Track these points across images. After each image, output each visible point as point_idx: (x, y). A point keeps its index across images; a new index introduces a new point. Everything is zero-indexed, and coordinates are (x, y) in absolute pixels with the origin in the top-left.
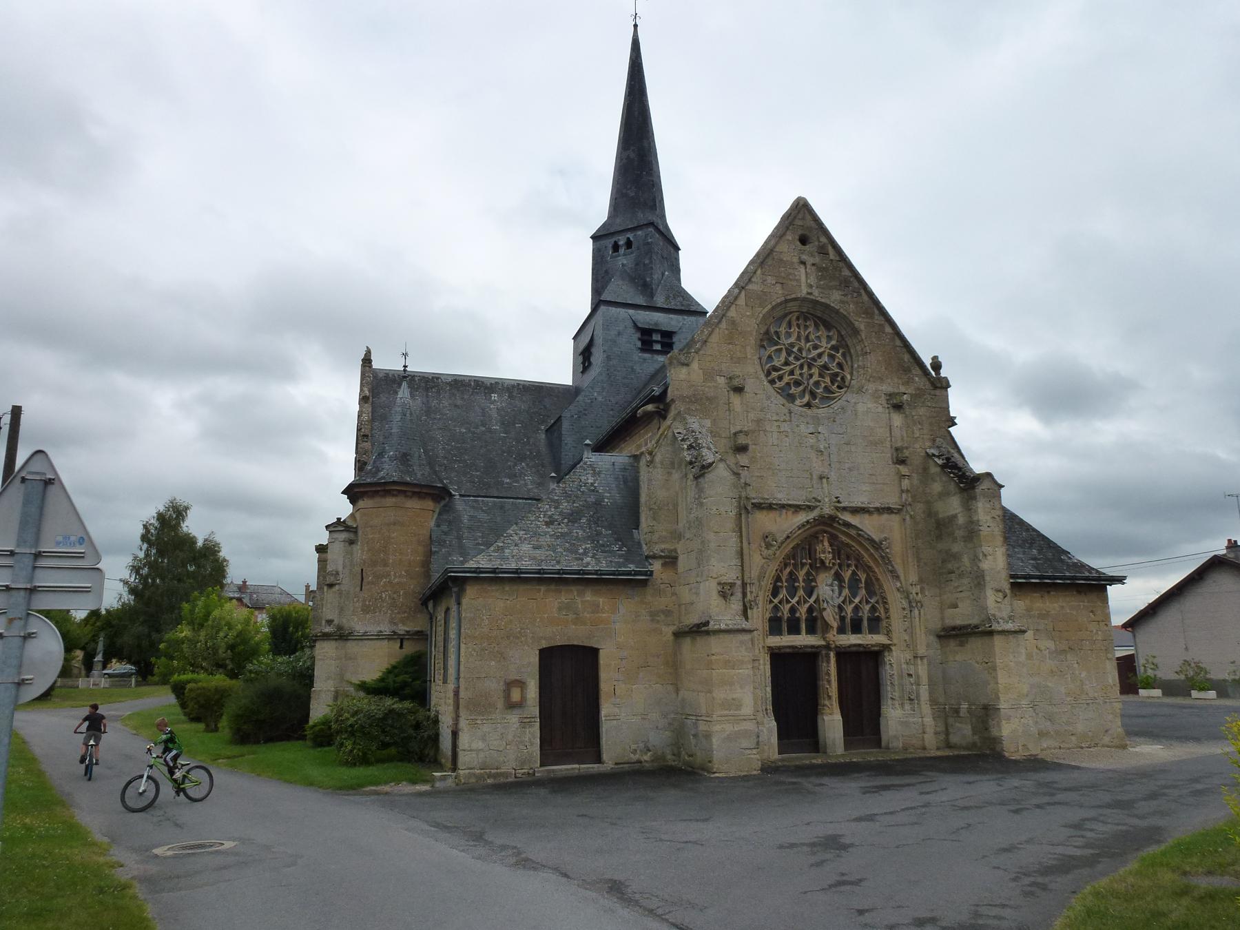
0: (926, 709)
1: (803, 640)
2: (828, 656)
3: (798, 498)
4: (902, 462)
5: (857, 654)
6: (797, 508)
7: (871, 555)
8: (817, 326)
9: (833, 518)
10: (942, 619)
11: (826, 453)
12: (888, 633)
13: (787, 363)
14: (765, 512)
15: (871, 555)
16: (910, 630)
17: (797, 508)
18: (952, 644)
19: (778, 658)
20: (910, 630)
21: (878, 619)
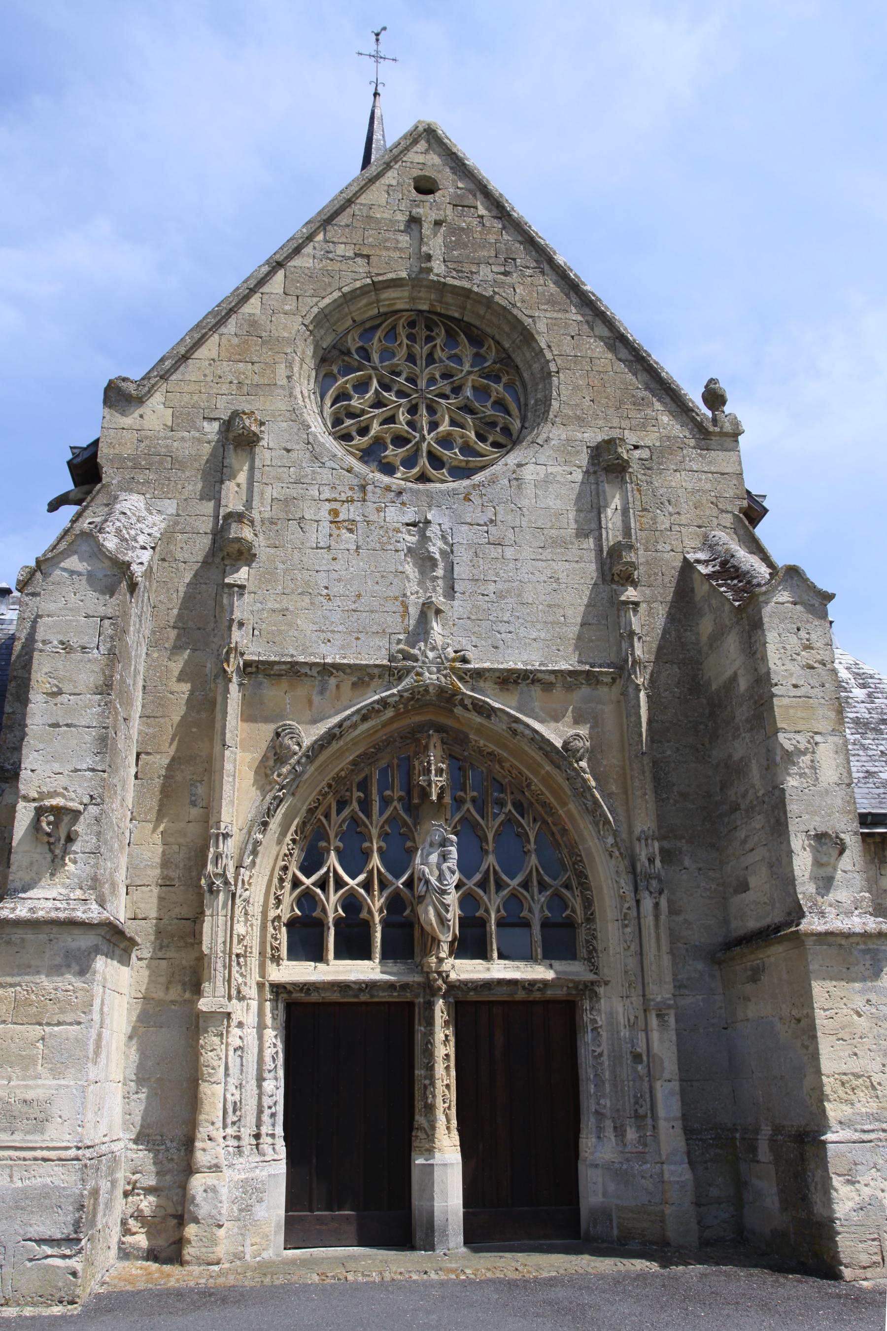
6: (362, 676)
8: (451, 336)
10: (726, 922)
12: (591, 959)
13: (379, 403)
14: (285, 684)
21: (570, 925)
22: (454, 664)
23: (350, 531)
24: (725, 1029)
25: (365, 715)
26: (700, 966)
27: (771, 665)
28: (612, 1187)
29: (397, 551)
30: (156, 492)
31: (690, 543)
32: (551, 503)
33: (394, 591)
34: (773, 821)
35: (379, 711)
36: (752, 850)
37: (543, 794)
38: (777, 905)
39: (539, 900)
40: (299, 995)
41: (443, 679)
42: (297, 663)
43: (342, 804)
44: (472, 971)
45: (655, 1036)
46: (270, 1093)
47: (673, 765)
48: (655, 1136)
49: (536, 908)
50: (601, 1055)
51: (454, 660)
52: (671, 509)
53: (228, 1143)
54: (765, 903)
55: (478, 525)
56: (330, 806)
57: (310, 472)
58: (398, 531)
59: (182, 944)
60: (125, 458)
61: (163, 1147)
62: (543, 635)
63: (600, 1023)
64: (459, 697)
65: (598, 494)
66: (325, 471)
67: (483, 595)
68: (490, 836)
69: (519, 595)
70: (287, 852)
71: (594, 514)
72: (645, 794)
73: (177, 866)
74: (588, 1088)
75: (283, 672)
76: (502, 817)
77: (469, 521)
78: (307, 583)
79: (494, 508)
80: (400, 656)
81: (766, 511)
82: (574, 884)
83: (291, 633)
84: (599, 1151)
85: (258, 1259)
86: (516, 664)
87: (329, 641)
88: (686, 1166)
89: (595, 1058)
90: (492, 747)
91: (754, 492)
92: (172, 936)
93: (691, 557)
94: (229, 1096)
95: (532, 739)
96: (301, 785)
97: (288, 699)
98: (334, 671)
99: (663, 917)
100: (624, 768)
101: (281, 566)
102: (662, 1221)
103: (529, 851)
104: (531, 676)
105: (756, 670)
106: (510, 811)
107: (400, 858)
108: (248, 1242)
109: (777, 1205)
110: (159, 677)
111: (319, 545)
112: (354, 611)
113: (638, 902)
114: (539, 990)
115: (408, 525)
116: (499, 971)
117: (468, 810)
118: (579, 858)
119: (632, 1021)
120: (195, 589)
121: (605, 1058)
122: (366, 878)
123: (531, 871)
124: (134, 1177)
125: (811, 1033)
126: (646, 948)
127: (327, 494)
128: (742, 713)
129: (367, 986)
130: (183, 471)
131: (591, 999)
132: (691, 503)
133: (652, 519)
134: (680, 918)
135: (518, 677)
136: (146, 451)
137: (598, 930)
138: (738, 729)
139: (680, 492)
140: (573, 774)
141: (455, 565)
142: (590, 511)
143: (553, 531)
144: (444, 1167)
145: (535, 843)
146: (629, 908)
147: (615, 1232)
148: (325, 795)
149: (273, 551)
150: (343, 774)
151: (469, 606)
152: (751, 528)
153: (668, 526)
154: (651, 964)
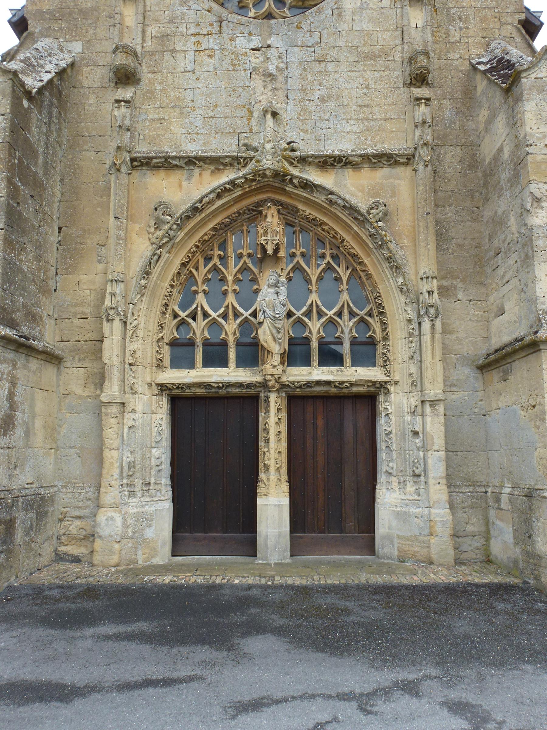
0: (438, 492)
1: (232, 374)
2: (267, 401)
3: (227, 146)
4: (420, 79)
5: (326, 398)
6: (216, 163)
7: (356, 237)
9: (280, 176)
11: (281, 78)
14: (162, 173)
15: (356, 237)
16: (417, 356)
17: (216, 163)
18: (495, 375)
19: (183, 405)
20: (417, 356)
21: (372, 343)
22: (285, 153)
23: (210, 56)
24: (485, 415)
25: (221, 192)
26: (467, 371)
27: (528, 129)
28: (394, 523)
29: (245, 70)
30: (67, 37)
31: (475, 51)
32: (364, 26)
33: (243, 101)
34: (523, 256)
35: (230, 190)
36: (508, 281)
37: (353, 248)
38: (524, 321)
39: (348, 325)
40: (177, 391)
41: (276, 164)
42: (169, 157)
43: (208, 259)
44: (298, 375)
45: (428, 419)
46: (157, 457)
47: (452, 224)
48: (427, 489)
49: (346, 330)
50: (390, 433)
51: (285, 150)
52: (461, 25)
53: (125, 489)
54: (515, 321)
55: (307, 47)
56: (198, 261)
57: (180, 14)
58: (246, 55)
59: (93, 358)
60: (44, 12)
61: (84, 491)
62: (355, 129)
63: (390, 411)
64: (289, 177)
65: (402, 16)
66: (192, 12)
67: (309, 100)
68: (314, 280)
69: (338, 99)
70: (167, 294)
71: (399, 32)
72: (428, 244)
73: (89, 305)
74: (382, 456)
75: (160, 164)
76: (323, 266)
77: (300, 44)
78: (179, 99)
79: (320, 32)
80: (244, 148)
81: (542, 24)
82: (375, 313)
83: (166, 136)
84: (389, 499)
85: (147, 563)
86: (333, 151)
87: (195, 141)
88: (448, 511)
89: (387, 434)
90: (315, 214)
91: (532, 9)
92: (87, 352)
93: (474, 62)
94: (124, 458)
95: (343, 206)
96: (175, 246)
97: (165, 184)
98: (197, 162)
99: (438, 336)
100: (414, 228)
101: (159, 87)
102: (429, 547)
103: (342, 290)
104: (344, 159)
105: (516, 137)
106: (329, 262)
107: (249, 296)
108: (140, 552)
109: (512, 540)
110: (73, 173)
111: (187, 70)
112: (213, 118)
113: (420, 324)
114: (346, 387)
115: (253, 50)
116: (318, 374)
117: (298, 262)
118: (378, 294)
119: (413, 410)
120: (97, 107)
121: (393, 436)
122: (224, 311)
123: (343, 306)
124: (65, 510)
125: (542, 417)
126: (424, 357)
127: (193, 30)
128: (505, 176)
129: (223, 386)
130: (86, 19)
131: (385, 394)
132: (478, 19)
133: (445, 34)
134: (453, 337)
135: (334, 161)
136: (59, 6)
137: (391, 345)
138: (502, 189)
139: (470, 11)
140: (374, 231)
141: (289, 79)
142: (396, 30)
143: (365, 48)
144: (273, 505)
145: (347, 284)
146: (413, 329)
147: (396, 553)
148: (194, 253)
149: (152, 76)
150: (206, 238)
151: (299, 109)
152: (531, 42)
153: (457, 38)
154: (427, 368)
